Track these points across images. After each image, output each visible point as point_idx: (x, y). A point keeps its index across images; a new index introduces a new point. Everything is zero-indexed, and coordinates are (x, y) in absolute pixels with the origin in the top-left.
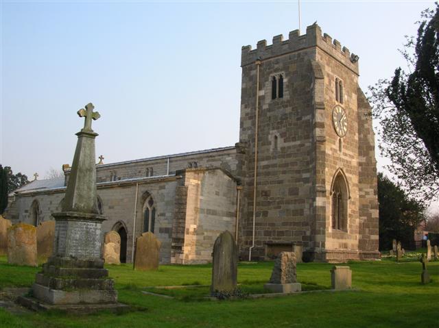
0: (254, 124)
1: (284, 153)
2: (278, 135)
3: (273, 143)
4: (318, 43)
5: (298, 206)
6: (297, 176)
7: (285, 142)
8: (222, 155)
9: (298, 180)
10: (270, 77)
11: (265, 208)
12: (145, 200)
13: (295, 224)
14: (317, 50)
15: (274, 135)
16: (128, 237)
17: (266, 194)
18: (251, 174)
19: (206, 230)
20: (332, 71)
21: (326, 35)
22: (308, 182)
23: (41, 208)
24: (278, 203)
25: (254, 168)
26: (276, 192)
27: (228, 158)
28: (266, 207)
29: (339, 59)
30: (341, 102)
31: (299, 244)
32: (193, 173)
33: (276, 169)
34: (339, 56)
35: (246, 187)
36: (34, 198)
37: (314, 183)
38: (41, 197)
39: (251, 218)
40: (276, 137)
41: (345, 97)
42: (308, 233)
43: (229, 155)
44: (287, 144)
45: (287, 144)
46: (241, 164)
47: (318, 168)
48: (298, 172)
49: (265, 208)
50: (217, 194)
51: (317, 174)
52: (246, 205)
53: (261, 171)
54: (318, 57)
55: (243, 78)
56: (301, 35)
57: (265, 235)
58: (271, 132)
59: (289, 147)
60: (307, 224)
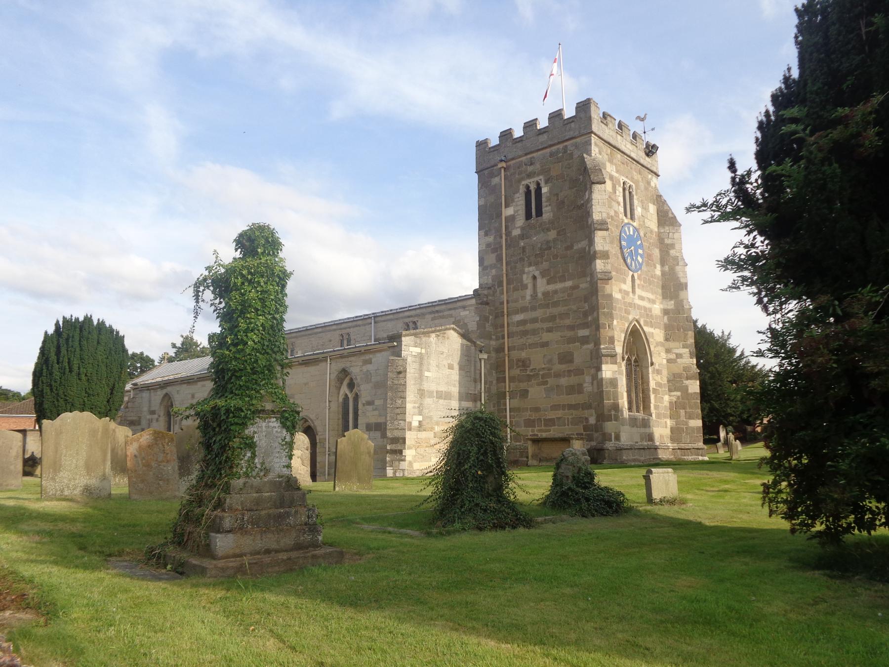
0: (499, 259)
2: (537, 273)
3: (530, 286)
5: (573, 380)
6: (569, 334)
7: (548, 283)
8: (455, 309)
10: (521, 187)
11: (523, 385)
12: (342, 383)
13: (571, 407)
14: (594, 139)
15: (531, 275)
17: (524, 364)
18: (500, 334)
21: (605, 116)
22: (587, 343)
24: (543, 376)
26: (537, 359)
27: (464, 313)
28: (525, 384)
30: (632, 218)
31: (580, 437)
32: (412, 338)
33: (537, 325)
34: (625, 144)
35: (493, 354)
36: (164, 391)
37: (597, 343)
38: (177, 388)
39: (502, 401)
40: (534, 278)
41: (638, 211)
42: (592, 421)
43: (464, 307)
44: (551, 288)
45: (551, 288)
46: (484, 319)
47: (602, 320)
48: (572, 328)
49: (523, 385)
51: (602, 330)
52: (495, 382)
53: (514, 329)
54: (595, 150)
58: (526, 270)
59: (556, 292)
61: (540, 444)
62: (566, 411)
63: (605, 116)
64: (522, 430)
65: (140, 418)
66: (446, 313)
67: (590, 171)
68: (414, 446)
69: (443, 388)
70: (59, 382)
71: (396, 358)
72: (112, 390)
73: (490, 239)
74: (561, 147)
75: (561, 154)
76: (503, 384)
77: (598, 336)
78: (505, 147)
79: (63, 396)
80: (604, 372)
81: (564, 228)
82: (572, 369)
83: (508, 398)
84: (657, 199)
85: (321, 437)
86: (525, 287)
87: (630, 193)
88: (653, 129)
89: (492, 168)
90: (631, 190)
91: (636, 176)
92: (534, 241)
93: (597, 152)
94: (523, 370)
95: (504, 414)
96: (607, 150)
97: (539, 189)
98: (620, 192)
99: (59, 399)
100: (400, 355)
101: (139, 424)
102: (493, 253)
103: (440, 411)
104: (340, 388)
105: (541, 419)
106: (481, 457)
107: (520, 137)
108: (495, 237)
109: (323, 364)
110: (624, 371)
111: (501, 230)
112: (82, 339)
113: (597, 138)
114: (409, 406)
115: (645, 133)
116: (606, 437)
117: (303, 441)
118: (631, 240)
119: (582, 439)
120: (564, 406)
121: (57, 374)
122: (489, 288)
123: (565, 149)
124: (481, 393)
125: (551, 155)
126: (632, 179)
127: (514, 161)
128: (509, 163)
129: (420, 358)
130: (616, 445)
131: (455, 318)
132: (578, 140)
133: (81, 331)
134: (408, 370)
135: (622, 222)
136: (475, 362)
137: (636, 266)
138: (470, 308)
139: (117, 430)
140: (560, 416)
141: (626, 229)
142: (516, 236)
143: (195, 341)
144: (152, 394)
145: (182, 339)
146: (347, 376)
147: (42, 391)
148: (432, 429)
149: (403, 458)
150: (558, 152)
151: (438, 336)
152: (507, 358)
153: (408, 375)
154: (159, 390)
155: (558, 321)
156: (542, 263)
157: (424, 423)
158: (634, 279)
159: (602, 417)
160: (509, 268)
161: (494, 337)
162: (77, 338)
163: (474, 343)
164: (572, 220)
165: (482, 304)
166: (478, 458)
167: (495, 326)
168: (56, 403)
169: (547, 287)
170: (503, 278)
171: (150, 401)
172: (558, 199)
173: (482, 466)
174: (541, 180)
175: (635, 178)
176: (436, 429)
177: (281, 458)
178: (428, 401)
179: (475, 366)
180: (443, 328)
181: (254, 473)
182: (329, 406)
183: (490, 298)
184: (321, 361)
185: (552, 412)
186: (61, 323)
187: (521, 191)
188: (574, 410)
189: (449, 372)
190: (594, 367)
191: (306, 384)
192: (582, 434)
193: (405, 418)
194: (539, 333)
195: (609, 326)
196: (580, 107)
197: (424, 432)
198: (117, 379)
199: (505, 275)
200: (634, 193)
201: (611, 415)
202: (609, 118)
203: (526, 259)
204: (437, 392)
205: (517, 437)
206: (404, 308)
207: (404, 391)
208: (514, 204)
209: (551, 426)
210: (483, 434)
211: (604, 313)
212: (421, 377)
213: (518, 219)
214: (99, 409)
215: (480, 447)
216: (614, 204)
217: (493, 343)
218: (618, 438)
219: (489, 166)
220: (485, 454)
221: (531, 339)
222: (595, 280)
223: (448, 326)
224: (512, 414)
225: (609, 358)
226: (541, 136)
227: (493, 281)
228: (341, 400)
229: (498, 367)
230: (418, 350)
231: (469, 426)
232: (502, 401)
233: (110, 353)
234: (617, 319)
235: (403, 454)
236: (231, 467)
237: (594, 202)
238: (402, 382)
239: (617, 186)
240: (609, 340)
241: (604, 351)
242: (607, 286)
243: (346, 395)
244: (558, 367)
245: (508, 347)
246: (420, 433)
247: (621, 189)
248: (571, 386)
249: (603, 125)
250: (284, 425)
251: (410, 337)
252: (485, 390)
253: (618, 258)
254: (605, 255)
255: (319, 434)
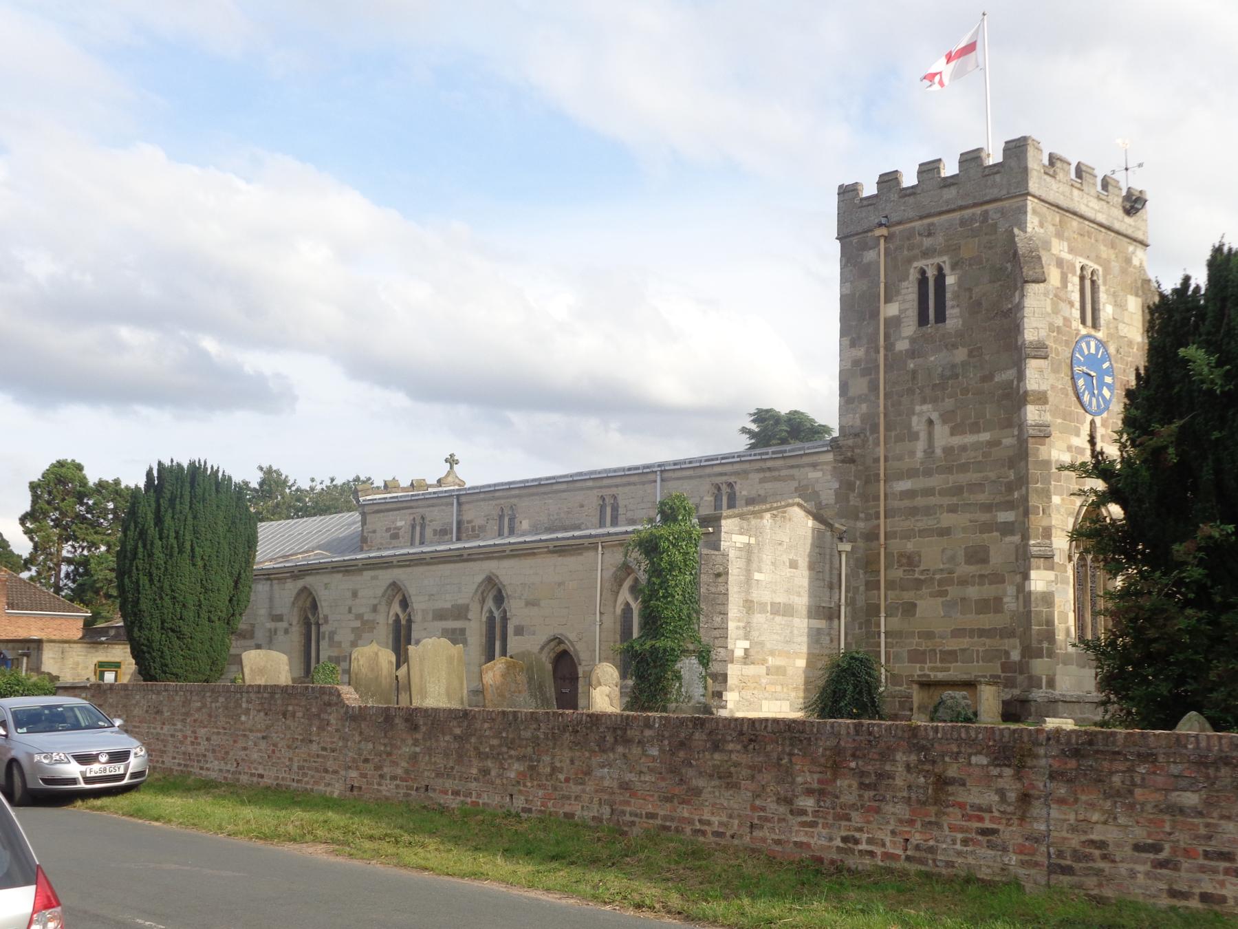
0: (874, 387)
1: (952, 461)
2: (935, 416)
3: (923, 436)
4: (1033, 186)
5: (988, 591)
6: (984, 517)
7: (952, 434)
8: (798, 466)
9: (987, 528)
10: (912, 271)
11: (908, 596)
12: (621, 585)
13: (982, 633)
14: (1031, 203)
15: (924, 419)
16: (580, 675)
17: (910, 561)
18: (872, 511)
19: (772, 653)
20: (1071, 251)
21: (1053, 159)
22: (1012, 533)
23: (324, 608)
24: (941, 583)
25: (877, 498)
26: (932, 554)
27: (813, 475)
28: (912, 593)
29: (1089, 213)
30: (1095, 326)
31: (994, 680)
32: (737, 520)
33: (933, 501)
34: (1087, 204)
35: (861, 544)
36: (300, 584)
37: (1025, 537)
38: (326, 579)
39: (874, 620)
40: (930, 422)
41: (1107, 311)
42: (1015, 656)
43: (814, 466)
44: (957, 441)
45: (957, 441)
46: (846, 486)
47: (1033, 501)
48: (988, 508)
49: (908, 596)
50: (793, 565)
51: (1032, 517)
52: (862, 588)
53: (896, 504)
54: (1032, 222)
55: (843, 267)
56: (991, 161)
57: (910, 661)
58: (918, 408)
59: (964, 448)
60: (1011, 634)
61: (931, 691)
62: (976, 639)
63: (1053, 159)
64: (898, 668)
65: (253, 625)
66: (784, 473)
67: (1022, 259)
68: (737, 686)
69: (781, 598)
70: (163, 569)
71: (713, 552)
72: (236, 583)
73: (860, 353)
74: (979, 212)
75: (978, 224)
76: (875, 592)
77: (1027, 525)
78: (886, 200)
79: (169, 592)
80: (1033, 583)
81: (978, 345)
82: (986, 573)
83: (883, 614)
84: (1142, 285)
85: (586, 669)
86: (914, 437)
87: (1093, 282)
88: (1140, 165)
89: (865, 235)
90: (1095, 278)
91: (1105, 252)
92: (931, 361)
93: (1036, 224)
94: (909, 571)
95: (877, 640)
96: (1055, 217)
97: (940, 278)
98: (1074, 285)
99: (164, 595)
100: (717, 548)
101: (252, 637)
102: (863, 375)
103: (778, 633)
104: (618, 593)
105: (935, 650)
106: (857, 696)
107: (913, 187)
108: (867, 352)
109: (591, 554)
110: (1072, 577)
111: (877, 340)
112: (194, 501)
113: (1036, 201)
114: (732, 625)
115: (1127, 169)
116: (1034, 682)
117: (612, 675)
118: (1092, 361)
119: (996, 684)
120: (972, 631)
121: (159, 556)
122: (856, 435)
123: (985, 214)
124: (839, 606)
125: (963, 223)
126: (1098, 260)
127: (901, 227)
128: (893, 229)
129: (748, 550)
130: (1049, 695)
131: (799, 482)
132: (1006, 204)
133: (192, 486)
134: (730, 571)
135: (1077, 334)
136: (832, 556)
137: (1098, 405)
138: (825, 467)
139: (380, 654)
140: (965, 647)
141: (1084, 345)
142: (901, 352)
143: (284, 477)
144: (276, 587)
145: (261, 475)
146: (629, 574)
147: (137, 582)
148: (764, 661)
149: (723, 703)
150: (972, 219)
151: (775, 516)
152: (882, 550)
153: (731, 578)
154: (288, 580)
155: (965, 495)
156: (943, 400)
157: (752, 652)
158: (1095, 427)
159: (1030, 652)
160: (889, 404)
161: (862, 515)
162: (187, 498)
163: (830, 526)
164: (993, 334)
165: (843, 461)
166: (853, 697)
167: (864, 497)
168: (159, 601)
169: (950, 440)
170: (879, 419)
171: (271, 599)
172: (971, 298)
173: (857, 703)
174: (944, 262)
175: (1104, 256)
176: (770, 662)
177: (698, 688)
178: (759, 619)
179: (831, 563)
180: (783, 503)
181: (681, 700)
182: (600, 621)
183: (857, 451)
184: (587, 549)
185: (954, 640)
186: (155, 473)
187: (911, 278)
188: (988, 637)
189: (790, 572)
190: (1020, 573)
191: (560, 584)
192: (999, 677)
193: (727, 643)
194: (935, 514)
195: (1043, 510)
196: (1009, 149)
197: (752, 666)
198: (243, 565)
199: (882, 416)
200: (1100, 282)
201: (1041, 649)
202: (1059, 164)
203: (918, 391)
204: (772, 604)
205: (894, 679)
206: (712, 460)
207: (725, 604)
208: (900, 298)
209: (951, 662)
210: (859, 673)
211: (1036, 490)
212: (748, 579)
213: (905, 324)
214: (220, 613)
215: (855, 686)
216: (1064, 306)
217: (861, 525)
218: (1051, 683)
219: (860, 229)
220: (860, 693)
221: (924, 522)
222: (1025, 437)
223: (790, 501)
224: (889, 640)
225: (1042, 559)
226: (946, 190)
227: (862, 423)
228: (619, 611)
229: (867, 564)
230: (744, 539)
231: (845, 665)
232: (874, 620)
233: (234, 523)
234: (1061, 495)
235: (724, 698)
236: (666, 694)
237: (1027, 312)
238: (722, 589)
239: (1070, 275)
240: (1043, 532)
241: (1034, 550)
242: (1042, 448)
243: (628, 604)
244: (965, 569)
245: (885, 533)
246: (746, 667)
247: (1076, 280)
248: (985, 600)
249: (1048, 178)
250: (701, 662)
251: (733, 520)
252: (846, 601)
253: (1067, 395)
254: (1042, 398)
255: (584, 663)
